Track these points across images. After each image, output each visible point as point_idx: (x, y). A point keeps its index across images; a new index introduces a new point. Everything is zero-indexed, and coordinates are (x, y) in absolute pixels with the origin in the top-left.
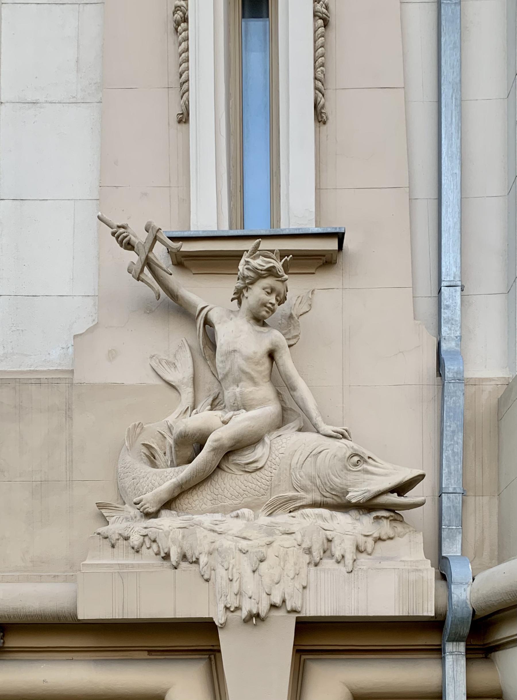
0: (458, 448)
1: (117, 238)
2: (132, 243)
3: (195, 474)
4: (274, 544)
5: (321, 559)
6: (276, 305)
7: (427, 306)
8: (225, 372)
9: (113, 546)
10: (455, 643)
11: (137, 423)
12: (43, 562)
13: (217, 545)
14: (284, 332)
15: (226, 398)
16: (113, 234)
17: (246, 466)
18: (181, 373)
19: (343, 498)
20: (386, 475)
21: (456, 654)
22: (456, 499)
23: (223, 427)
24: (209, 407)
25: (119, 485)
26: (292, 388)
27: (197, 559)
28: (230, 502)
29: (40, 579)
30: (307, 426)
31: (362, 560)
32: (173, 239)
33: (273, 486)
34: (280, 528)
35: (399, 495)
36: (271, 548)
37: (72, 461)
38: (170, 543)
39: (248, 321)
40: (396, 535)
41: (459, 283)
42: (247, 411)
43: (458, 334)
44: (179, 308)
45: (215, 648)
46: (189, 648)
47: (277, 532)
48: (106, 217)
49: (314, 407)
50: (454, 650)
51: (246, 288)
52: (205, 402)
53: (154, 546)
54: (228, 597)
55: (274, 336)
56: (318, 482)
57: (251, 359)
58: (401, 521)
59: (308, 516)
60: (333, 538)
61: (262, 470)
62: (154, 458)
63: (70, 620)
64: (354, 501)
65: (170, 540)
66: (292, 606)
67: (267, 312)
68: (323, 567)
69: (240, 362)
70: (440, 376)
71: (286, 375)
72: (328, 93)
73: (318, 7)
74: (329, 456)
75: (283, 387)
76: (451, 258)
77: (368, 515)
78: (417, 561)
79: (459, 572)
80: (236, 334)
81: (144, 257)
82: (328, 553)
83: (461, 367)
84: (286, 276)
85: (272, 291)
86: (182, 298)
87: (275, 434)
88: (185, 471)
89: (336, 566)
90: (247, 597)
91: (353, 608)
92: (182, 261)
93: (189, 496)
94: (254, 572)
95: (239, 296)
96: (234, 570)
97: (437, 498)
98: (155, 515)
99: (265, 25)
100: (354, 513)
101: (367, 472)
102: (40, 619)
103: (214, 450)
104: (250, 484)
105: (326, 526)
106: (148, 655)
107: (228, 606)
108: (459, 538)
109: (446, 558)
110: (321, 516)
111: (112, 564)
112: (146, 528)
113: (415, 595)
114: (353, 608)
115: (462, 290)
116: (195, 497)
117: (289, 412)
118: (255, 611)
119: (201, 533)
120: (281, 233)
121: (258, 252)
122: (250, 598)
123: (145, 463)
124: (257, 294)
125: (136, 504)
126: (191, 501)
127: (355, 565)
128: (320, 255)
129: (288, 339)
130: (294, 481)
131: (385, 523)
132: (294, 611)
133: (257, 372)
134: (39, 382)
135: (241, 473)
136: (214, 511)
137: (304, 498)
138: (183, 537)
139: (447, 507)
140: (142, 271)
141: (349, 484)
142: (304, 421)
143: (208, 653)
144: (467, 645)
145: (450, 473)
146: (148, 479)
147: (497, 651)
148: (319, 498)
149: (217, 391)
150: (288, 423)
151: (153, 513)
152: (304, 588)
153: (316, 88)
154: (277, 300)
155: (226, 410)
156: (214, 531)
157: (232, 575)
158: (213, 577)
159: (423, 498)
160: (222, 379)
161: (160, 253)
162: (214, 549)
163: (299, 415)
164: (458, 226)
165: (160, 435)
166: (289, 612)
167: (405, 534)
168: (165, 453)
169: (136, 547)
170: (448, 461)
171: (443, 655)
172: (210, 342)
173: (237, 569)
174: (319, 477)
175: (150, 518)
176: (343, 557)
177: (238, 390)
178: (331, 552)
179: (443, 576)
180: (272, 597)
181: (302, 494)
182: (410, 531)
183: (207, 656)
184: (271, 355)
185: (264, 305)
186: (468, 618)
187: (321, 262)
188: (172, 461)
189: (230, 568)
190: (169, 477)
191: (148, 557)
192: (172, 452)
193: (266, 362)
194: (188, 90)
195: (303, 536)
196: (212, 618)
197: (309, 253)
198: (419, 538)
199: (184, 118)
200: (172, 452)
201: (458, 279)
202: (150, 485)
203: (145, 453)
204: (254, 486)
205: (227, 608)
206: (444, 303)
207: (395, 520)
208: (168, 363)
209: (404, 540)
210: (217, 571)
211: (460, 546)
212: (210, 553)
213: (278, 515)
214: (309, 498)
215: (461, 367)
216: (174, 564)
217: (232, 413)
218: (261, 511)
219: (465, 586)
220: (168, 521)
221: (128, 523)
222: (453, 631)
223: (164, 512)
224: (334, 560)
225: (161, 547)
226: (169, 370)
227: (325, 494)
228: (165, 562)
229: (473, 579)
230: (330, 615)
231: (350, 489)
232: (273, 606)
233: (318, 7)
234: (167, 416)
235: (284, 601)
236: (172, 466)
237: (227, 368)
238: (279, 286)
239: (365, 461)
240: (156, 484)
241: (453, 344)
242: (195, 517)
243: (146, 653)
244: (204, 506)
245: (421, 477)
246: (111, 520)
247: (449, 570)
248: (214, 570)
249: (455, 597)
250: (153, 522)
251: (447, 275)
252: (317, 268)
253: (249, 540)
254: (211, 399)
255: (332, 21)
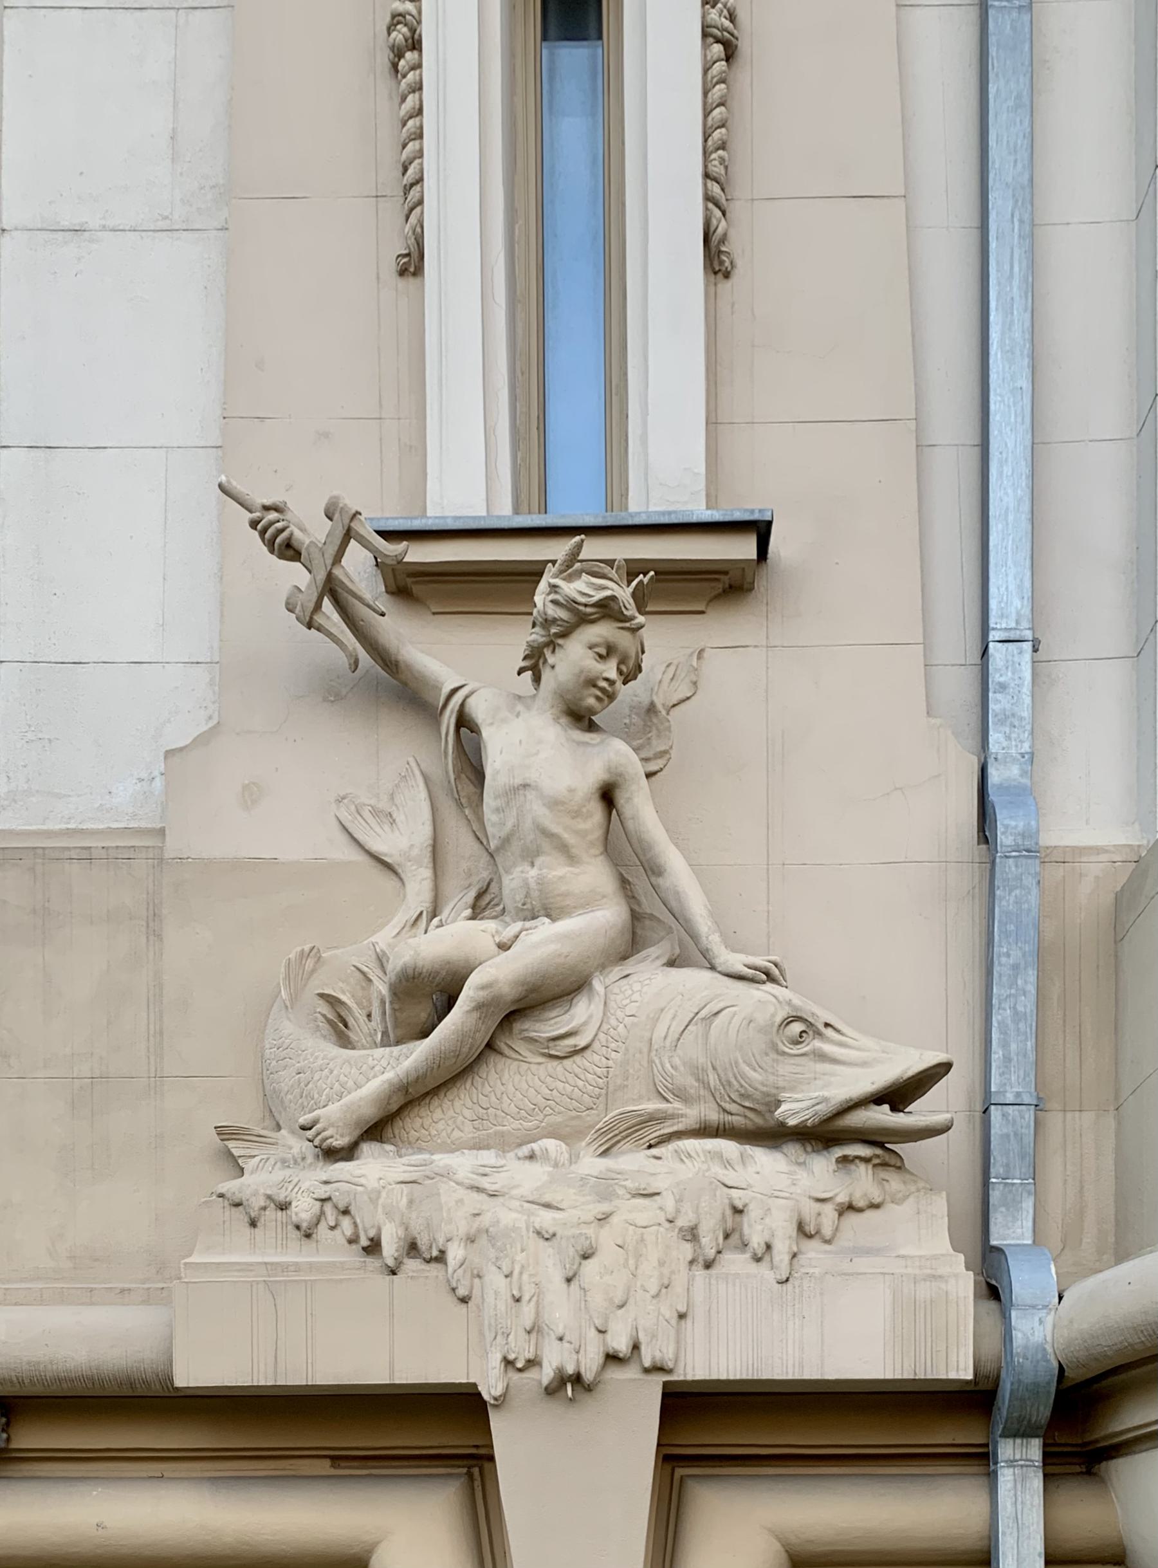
0: (1027, 1004)
1: (263, 533)
2: (295, 544)
3: (438, 1061)
4: (615, 1219)
5: (719, 1252)
6: (619, 684)
7: (957, 685)
8: (503, 834)
9: (253, 1224)
10: (1018, 1441)
11: (307, 948)
12: (96, 1260)
13: (486, 1220)
14: (635, 743)
15: (506, 892)
16: (254, 524)
17: (551, 1044)
18: (406, 835)
19: (768, 1115)
20: (864, 1064)
21: (1022, 1466)
22: (1022, 1117)
23: (499, 957)
24: (468, 912)
25: (267, 1087)
26: (654, 870)
27: (442, 1252)
28: (516, 1124)
29: (90, 1298)
30: (688, 954)
31: (812, 1255)
32: (388, 535)
33: (611, 1088)
34: (628, 1183)
35: (894, 1109)
36: (607, 1228)
37: (161, 1033)
38: (380, 1217)
39: (556, 720)
40: (888, 1198)
41: (1028, 635)
42: (554, 920)
43: (1026, 747)
44: (401, 691)
45: (482, 1451)
46: (424, 1452)
47: (621, 1192)
48: (238, 486)
49: (704, 912)
50: (1018, 1457)
51: (552, 644)
52: (459, 901)
53: (346, 1222)
54: (511, 1337)
55: (613, 753)
56: (712, 1079)
57: (563, 803)
58: (899, 1168)
59: (689, 1156)
60: (745, 1206)
61: (588, 1053)
62: (346, 1026)
63: (156, 1390)
64: (792, 1122)
65: (380, 1210)
66: (653, 1358)
67: (598, 699)
68: (724, 1270)
69: (537, 810)
70: (987, 841)
71: (640, 840)
72: (735, 209)
73: (713, 15)
74: (736, 1021)
75: (633, 867)
76: (1011, 578)
77: (825, 1153)
78: (935, 1257)
79: (1028, 1280)
80: (528, 748)
81: (321, 576)
82: (734, 1239)
83: (1033, 823)
84: (641, 619)
85: (608, 651)
86: (409, 667)
87: (617, 972)
88: (415, 1055)
89: (753, 1268)
90: (553, 1337)
91: (790, 1363)
92: (407, 586)
93: (424, 1112)
94: (569, 1280)
95: (534, 663)
96: (525, 1277)
97: (978, 1115)
98: (348, 1153)
99: (594, 57)
100: (793, 1149)
101: (822, 1057)
102: (90, 1386)
103: (480, 1007)
104: (560, 1085)
105: (730, 1177)
106: (332, 1466)
107: (511, 1357)
108: (1028, 1204)
109: (998, 1250)
110: (718, 1156)
111: (251, 1264)
112: (326, 1183)
113: (929, 1334)
114: (790, 1363)
115: (1035, 650)
116: (438, 1114)
117: (647, 922)
118: (570, 1370)
119: (449, 1194)
120: (630, 522)
121: (577, 565)
122: (561, 1339)
123: (325, 1037)
124: (575, 657)
125: (304, 1128)
126: (427, 1122)
127: (796, 1267)
128: (717, 571)
129: (645, 760)
130: (658, 1078)
131: (863, 1172)
132: (658, 1369)
133: (577, 832)
134: (87, 857)
135: (540, 1059)
136: (479, 1146)
137: (682, 1116)
138: (411, 1202)
139: (1002, 1136)
140: (318, 606)
141: (781, 1084)
142: (681, 944)
143: (465, 1462)
144: (1045, 1445)
145: (1007, 1059)
146: (331, 1072)
147: (1113, 1458)
148: (714, 1116)
149: (485, 875)
150: (644, 947)
151: (342, 1149)
152: (682, 1316)
153: (708, 198)
154: (620, 672)
155: (507, 919)
156: (479, 1190)
157: (520, 1289)
158: (476, 1293)
159: (948, 1116)
160: (498, 849)
161: (358, 567)
162: (479, 1231)
163: (670, 930)
164: (1026, 507)
165: (358, 974)
166: (647, 1371)
167: (906, 1197)
168: (369, 1016)
169: (304, 1225)
170: (1004, 1032)
171: (992, 1467)
172: (471, 766)
173: (531, 1275)
174: (714, 1068)
175: (337, 1161)
176: (769, 1247)
177: (533, 873)
178: (741, 1235)
179: (993, 1291)
180: (608, 1336)
181: (676, 1106)
182: (918, 1190)
183: (465, 1470)
184: (608, 796)
185: (592, 683)
186: (1048, 1383)
187: (719, 587)
188: (385, 1033)
189: (516, 1273)
190: (379, 1069)
191: (331, 1248)
192: (384, 1013)
193: (597, 810)
194: (420, 202)
195: (680, 1201)
196: (475, 1385)
197: (693, 567)
198: (939, 1205)
199: (411, 265)
200: (384, 1013)
201: (1025, 624)
202: (337, 1086)
203: (324, 1016)
204: (569, 1088)
205: (508, 1363)
206: (995, 678)
207: (885, 1165)
208: (375, 812)
209: (905, 1210)
210: (486, 1279)
211: (1030, 1224)
212: (471, 1240)
213: (623, 1153)
214: (692, 1115)
215: (1033, 823)
216: (391, 1262)
217: (519, 925)
218: (584, 1144)
219: (1043, 1313)
220: (375, 1167)
221: (287, 1172)
222: (1015, 1414)
223: (366, 1148)
224: (748, 1255)
225: (360, 1226)
226: (378, 829)
227: (727, 1106)
228: (369, 1260)
229: (1060, 1298)
230: (738, 1377)
231: (784, 1095)
232: (612, 1358)
233: (713, 15)
234: (374, 933)
235: (636, 1347)
236: (385, 1043)
237: (509, 824)
238: (624, 640)
239: (819, 1034)
240: (350, 1083)
241: (1014, 771)
242: (436, 1157)
243: (328, 1462)
244: (457, 1134)
245: (944, 1068)
246: (249, 1165)
247: (1005, 1278)
248: (479, 1276)
249: (1018, 1338)
250: (342, 1169)
251: (1002, 616)
252: (711, 601)
253: (558, 1209)
254: (472, 894)
255: (744, 46)
